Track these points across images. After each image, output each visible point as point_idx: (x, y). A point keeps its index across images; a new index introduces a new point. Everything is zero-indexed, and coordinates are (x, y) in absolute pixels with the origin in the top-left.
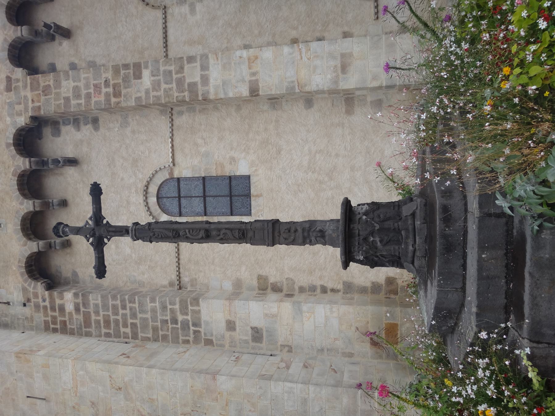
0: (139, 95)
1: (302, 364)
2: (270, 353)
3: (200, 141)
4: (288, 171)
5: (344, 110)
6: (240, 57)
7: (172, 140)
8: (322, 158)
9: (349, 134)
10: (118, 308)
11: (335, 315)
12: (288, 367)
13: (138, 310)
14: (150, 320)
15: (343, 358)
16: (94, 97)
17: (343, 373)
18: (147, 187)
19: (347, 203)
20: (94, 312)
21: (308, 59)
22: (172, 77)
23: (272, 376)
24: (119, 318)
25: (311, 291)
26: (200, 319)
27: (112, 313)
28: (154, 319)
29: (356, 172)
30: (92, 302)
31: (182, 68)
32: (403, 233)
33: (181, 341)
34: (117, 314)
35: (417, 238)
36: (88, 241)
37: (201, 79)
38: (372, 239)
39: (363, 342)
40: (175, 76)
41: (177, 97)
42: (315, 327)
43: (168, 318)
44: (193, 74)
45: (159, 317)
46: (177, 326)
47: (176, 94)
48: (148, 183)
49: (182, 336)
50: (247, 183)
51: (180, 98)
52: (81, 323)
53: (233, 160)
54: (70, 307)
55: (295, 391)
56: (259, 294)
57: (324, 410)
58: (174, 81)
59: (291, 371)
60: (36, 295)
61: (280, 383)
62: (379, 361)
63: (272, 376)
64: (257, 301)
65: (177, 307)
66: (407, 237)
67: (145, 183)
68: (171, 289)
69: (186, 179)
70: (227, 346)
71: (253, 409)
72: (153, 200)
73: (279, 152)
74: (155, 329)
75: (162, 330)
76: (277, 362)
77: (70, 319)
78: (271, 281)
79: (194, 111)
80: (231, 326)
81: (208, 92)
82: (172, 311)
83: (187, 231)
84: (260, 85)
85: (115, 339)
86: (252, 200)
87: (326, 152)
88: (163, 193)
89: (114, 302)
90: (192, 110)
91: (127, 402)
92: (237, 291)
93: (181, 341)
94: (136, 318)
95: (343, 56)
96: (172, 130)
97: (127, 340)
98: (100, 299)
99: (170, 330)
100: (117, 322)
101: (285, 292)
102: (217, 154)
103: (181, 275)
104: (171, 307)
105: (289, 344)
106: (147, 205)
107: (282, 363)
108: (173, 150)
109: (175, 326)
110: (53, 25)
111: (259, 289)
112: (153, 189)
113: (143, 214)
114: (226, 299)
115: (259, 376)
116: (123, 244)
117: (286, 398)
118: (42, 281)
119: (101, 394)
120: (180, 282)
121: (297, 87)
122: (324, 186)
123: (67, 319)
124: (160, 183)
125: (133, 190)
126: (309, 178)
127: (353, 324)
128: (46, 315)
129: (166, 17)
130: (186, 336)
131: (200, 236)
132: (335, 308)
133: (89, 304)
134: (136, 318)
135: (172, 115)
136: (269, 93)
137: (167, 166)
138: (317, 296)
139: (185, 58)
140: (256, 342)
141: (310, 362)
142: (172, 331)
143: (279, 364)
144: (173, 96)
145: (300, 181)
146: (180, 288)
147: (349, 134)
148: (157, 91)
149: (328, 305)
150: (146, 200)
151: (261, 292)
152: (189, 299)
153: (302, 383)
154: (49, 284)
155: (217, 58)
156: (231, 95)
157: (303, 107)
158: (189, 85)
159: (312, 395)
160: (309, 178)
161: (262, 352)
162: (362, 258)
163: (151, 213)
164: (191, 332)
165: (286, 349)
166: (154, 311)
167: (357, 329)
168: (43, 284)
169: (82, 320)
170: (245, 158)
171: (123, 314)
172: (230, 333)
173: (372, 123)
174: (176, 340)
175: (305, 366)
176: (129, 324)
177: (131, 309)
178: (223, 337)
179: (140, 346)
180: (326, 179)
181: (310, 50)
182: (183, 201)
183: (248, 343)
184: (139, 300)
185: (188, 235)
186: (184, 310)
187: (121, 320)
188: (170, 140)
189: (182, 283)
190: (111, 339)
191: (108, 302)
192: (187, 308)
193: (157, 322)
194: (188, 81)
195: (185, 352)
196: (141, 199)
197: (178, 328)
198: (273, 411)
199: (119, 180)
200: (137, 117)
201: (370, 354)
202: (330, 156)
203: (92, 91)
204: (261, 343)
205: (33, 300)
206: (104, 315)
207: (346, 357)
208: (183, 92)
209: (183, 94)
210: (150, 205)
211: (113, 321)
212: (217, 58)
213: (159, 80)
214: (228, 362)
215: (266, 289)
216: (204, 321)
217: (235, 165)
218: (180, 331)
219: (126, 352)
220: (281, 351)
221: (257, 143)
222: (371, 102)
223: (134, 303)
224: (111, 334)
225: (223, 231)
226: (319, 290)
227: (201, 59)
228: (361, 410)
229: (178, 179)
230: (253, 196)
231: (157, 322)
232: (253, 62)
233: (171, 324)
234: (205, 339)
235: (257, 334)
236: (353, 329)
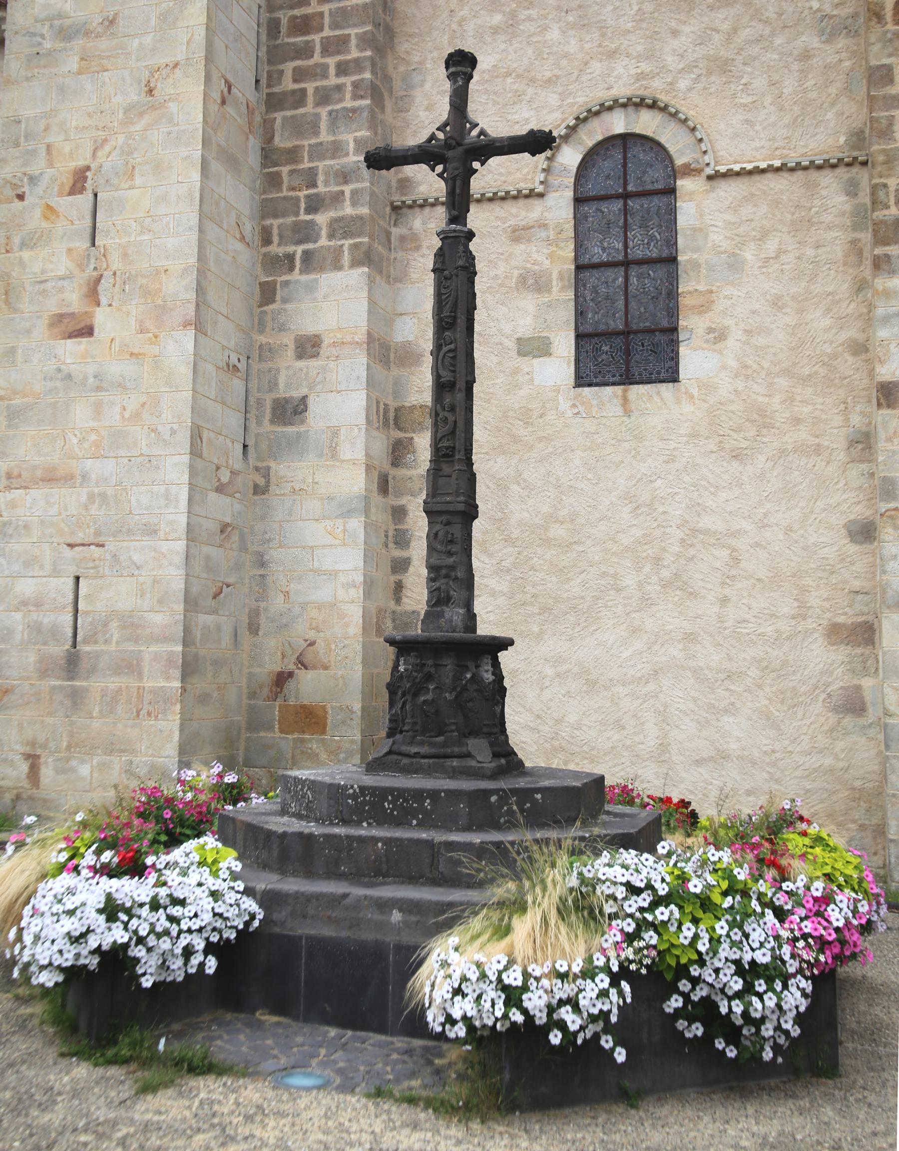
1: (228, 520)
2: (251, 442)
3: (772, 246)
4: (687, 479)
5: (841, 619)
7: (778, 170)
8: (718, 564)
9: (777, 631)
10: (339, 52)
11: (341, 594)
12: (220, 489)
13: (338, 106)
14: (313, 141)
15: (247, 610)
17: (215, 612)
18: (653, 105)
19: (505, 644)
23: (201, 457)
24: (317, 58)
25: (395, 536)
26: (321, 269)
27: (327, 38)
28: (318, 152)
29: (681, 646)
32: (441, 739)
33: (268, 222)
34: (326, 51)
35: (431, 761)
36: (438, 129)
38: (431, 687)
39: (283, 656)
41: (885, 186)
42: (311, 547)
43: (321, 189)
45: (321, 165)
46: (302, 211)
48: (664, 109)
49: (279, 227)
50: (659, 373)
53: (718, 336)
55: (171, 510)
56: (386, 411)
57: (136, 573)
59: (213, 496)
61: (186, 477)
62: (245, 691)
63: (201, 457)
64: (368, 409)
65: (348, 210)
66: (431, 745)
67: (663, 98)
69: (672, 212)
70: (263, 339)
71: (127, 415)
72: (618, 123)
73: (737, 456)
74: (293, 155)
75: (292, 172)
76: (231, 462)
78: (416, 439)
79: (856, 227)
80: (308, 347)
82: (338, 198)
83: (452, 346)
85: (264, 49)
86: (616, 388)
87: (733, 572)
88: (638, 152)
89: (353, 42)
90: (859, 219)
91: (121, 112)
92: (392, 355)
93: (268, 222)
94: (317, 104)
96: (805, 168)
97: (264, 81)
100: (306, 51)
101: (393, 472)
102: (736, 293)
103: (427, 210)
104: (347, 195)
105: (272, 488)
106: (605, 108)
107: (229, 474)
108: (750, 173)
109: (303, 205)
111: (397, 410)
112: (646, 123)
113: (581, 100)
114: (369, 334)
115: (198, 427)
116: (503, 46)
117: (156, 489)
119: (136, 43)
122: (647, 569)
124: (663, 140)
125: (645, 67)
126: (668, 530)
127: (322, 635)
130: (281, 236)
131: (443, 373)
132: (357, 594)
134: (317, 104)
135: (849, 165)
136: (882, 435)
137: (707, 159)
138: (383, 551)
140: (273, 409)
141: (235, 538)
142: (291, 198)
143: (227, 467)
144: (889, 176)
145: (661, 510)
146: (395, 209)
147: (777, 631)
149: (361, 579)
150: (616, 105)
151: (391, 415)
152: (366, 240)
153: (188, 523)
157: (852, 517)
159: (164, 546)
160: (668, 530)
161: (252, 424)
162: (402, 668)
163: (585, 120)
164: (290, 249)
165: (261, 481)
166: (337, 149)
167: (312, 644)
170: (723, 367)
171: (325, 67)
172: (292, 346)
173: (804, 688)
174: (268, 209)
175: (224, 528)
176: (303, 85)
177: (339, 88)
178: (282, 329)
179: (250, 123)
180: (665, 574)
182: (617, 206)
183: (270, 390)
185: (445, 349)
186: (342, 228)
187: (311, 62)
188: (777, 163)
189: (409, 211)
190: (264, 38)
191: (355, 26)
192: (346, 235)
193: (311, 160)
195: (243, 239)
196: (622, 90)
197: (297, 214)
198: (126, 460)
199: (673, 24)
200: (847, 64)
201: (258, 670)
202: (723, 583)
204: (272, 422)
206: (321, 14)
207: (250, 617)
210: (606, 116)
211: (307, 42)
214: (224, 348)
215: (398, 426)
216: (316, 280)
217: (707, 341)
218: (291, 219)
219: (234, 90)
220: (257, 469)
221: (761, 399)
222: (858, 688)
224: (276, 38)
225: (451, 418)
226: (398, 553)
228: (140, 651)
229: (671, 191)
230: (625, 391)
231: (311, 160)
233: (307, 197)
234: (274, 282)
235: (291, 411)
236: (311, 635)
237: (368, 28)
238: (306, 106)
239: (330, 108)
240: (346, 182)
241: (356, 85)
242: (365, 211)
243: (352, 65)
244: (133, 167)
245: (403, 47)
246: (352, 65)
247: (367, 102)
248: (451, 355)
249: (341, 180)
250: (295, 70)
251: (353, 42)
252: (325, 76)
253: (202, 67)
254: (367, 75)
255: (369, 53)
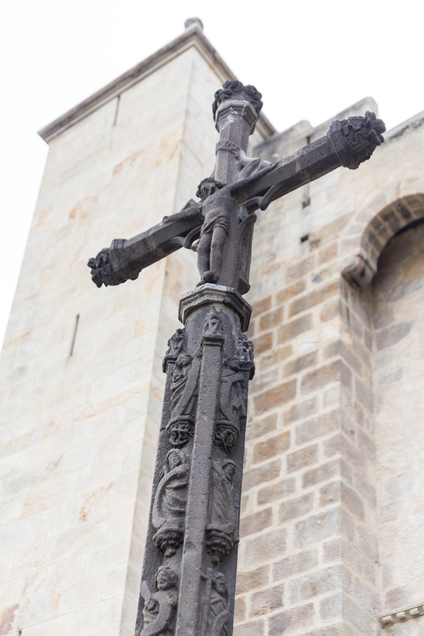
10: (306, 464)
14: (279, 558)
20: (294, 408)
24: (283, 475)
30: (319, 393)
34: (292, 466)
45: (286, 582)
52: (267, 384)
54: (302, 345)
60: (328, 255)
68: (383, 598)
75: (255, 595)
77: (276, 355)
83: (179, 469)
98: (328, 410)
99: (255, 619)
100: (272, 472)
104: (317, 607)
118: (366, 256)
120: (403, 620)
123: (275, 347)
128: (281, 297)
133: (313, 387)
134: (283, 520)
142: (254, 624)
154: (363, 274)
168: (357, 261)
169: (274, 385)
177: (306, 499)
184: (330, 513)
191: (323, 434)
205: (316, 252)
211: (273, 463)
223: (324, 502)
231: (276, 578)
233: (273, 619)
237: (337, 432)
238: (270, 525)
239: (296, 521)
240: (315, 594)
241: (324, 491)
242: (337, 621)
243: (320, 472)
244: (59, 595)
245: (384, 457)
246: (320, 472)
247: (338, 504)
248: (175, 484)
249: (309, 592)
250: (260, 493)
251: (321, 450)
252: (291, 490)
253: (136, 480)
254: (337, 478)
255: (338, 456)
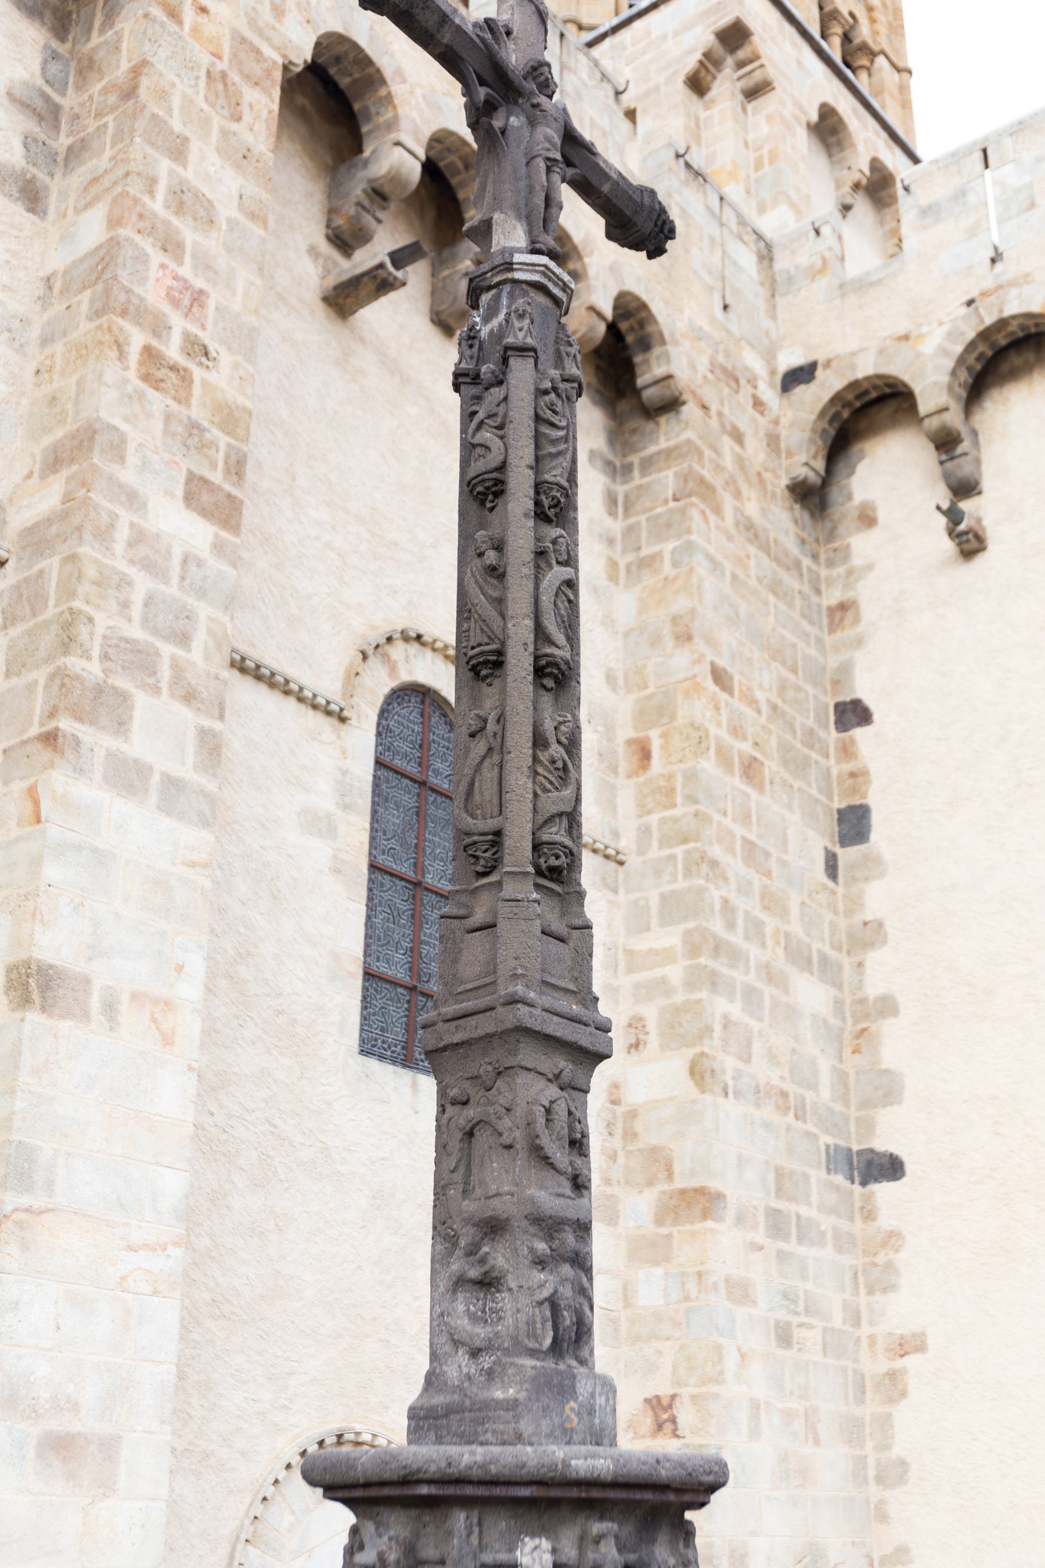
0: (132, 459)
6: (180, 968)
16: (163, 266)
21: (124, 1278)
22: (166, 638)
31: (189, 697)
37: (136, 761)
40: (167, 650)
41: (90, 620)
44: (158, 731)
47: (103, 622)
51: (83, 631)
58: (150, 639)
81: (80, 771)
84: (65, 1025)
95: (110, 1446)
110: (399, 274)
121: (25, 1201)
129: (315, 707)
139: (218, 726)
144: (98, 607)
148: (130, 545)
155: (193, 865)
156: (52, 871)
158: (124, 697)
181: (155, 1293)
194: (141, 699)
203: (185, 271)
208: (105, 657)
209: (96, 653)
212: (193, 865)
213: (167, 582)
227: (203, 793)
232: (154, 1020)
